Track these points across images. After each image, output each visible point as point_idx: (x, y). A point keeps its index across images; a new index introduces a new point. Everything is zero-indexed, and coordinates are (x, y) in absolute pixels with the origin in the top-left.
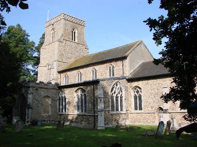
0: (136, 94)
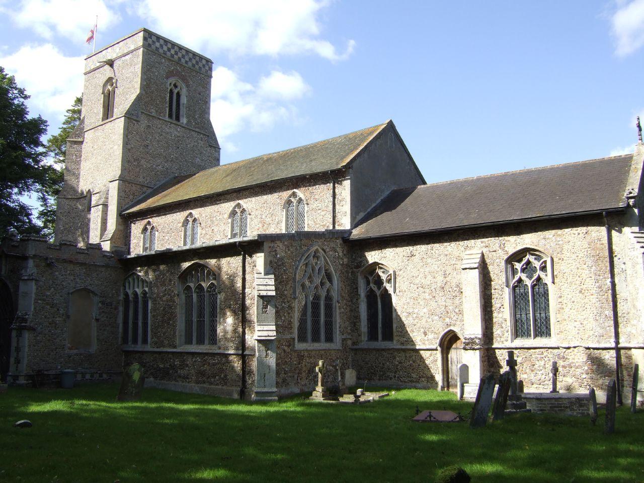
0: (375, 288)
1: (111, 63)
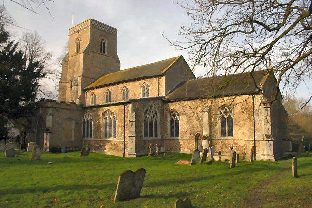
1: (78, 32)
